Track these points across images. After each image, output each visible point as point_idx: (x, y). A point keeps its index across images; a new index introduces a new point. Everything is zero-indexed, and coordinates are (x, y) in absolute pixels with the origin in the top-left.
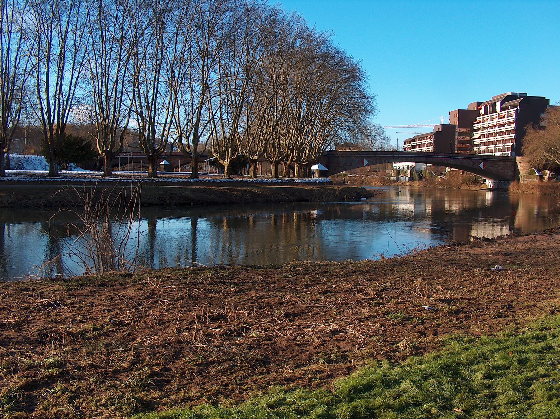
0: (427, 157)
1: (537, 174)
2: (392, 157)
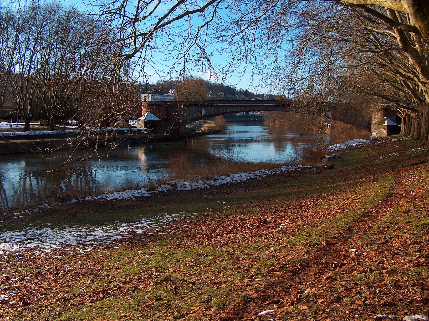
0: (268, 106)
1: (386, 124)
2: (230, 106)
